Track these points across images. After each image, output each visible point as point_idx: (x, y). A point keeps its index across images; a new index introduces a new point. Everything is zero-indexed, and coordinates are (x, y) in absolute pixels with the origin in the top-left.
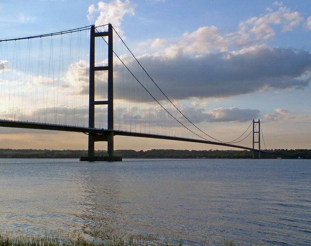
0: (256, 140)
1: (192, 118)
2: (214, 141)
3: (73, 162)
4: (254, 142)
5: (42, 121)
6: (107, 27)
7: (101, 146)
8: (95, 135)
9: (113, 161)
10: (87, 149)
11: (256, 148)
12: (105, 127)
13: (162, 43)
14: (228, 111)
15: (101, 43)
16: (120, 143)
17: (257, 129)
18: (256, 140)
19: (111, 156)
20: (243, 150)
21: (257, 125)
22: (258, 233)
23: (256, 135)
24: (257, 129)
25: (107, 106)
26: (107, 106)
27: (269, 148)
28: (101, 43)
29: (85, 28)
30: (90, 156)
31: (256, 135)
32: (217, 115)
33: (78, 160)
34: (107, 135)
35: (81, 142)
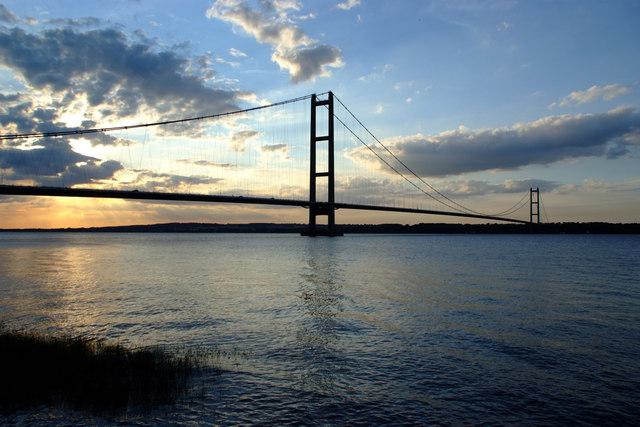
0: (535, 211)
1: (479, 190)
2: (464, 211)
3: (11, 240)
4: (532, 214)
5: (285, 196)
6: (327, 95)
7: (322, 220)
8: (315, 207)
9: (469, 233)
10: (307, 222)
11: (535, 221)
12: (325, 199)
13: (56, 116)
14: (521, 183)
15: (322, 113)
16: (342, 217)
17: (535, 200)
18: (535, 211)
19: (334, 231)
20: (507, 222)
21: (535, 194)
22: (507, 318)
23: (535, 206)
24: (535, 200)
25: (327, 178)
26: (327, 178)
27: (551, 220)
28: (322, 113)
29: (305, 98)
30: (310, 231)
31: (535, 206)
32: (508, 186)
33: (299, 235)
34: (329, 208)
35: (302, 216)
